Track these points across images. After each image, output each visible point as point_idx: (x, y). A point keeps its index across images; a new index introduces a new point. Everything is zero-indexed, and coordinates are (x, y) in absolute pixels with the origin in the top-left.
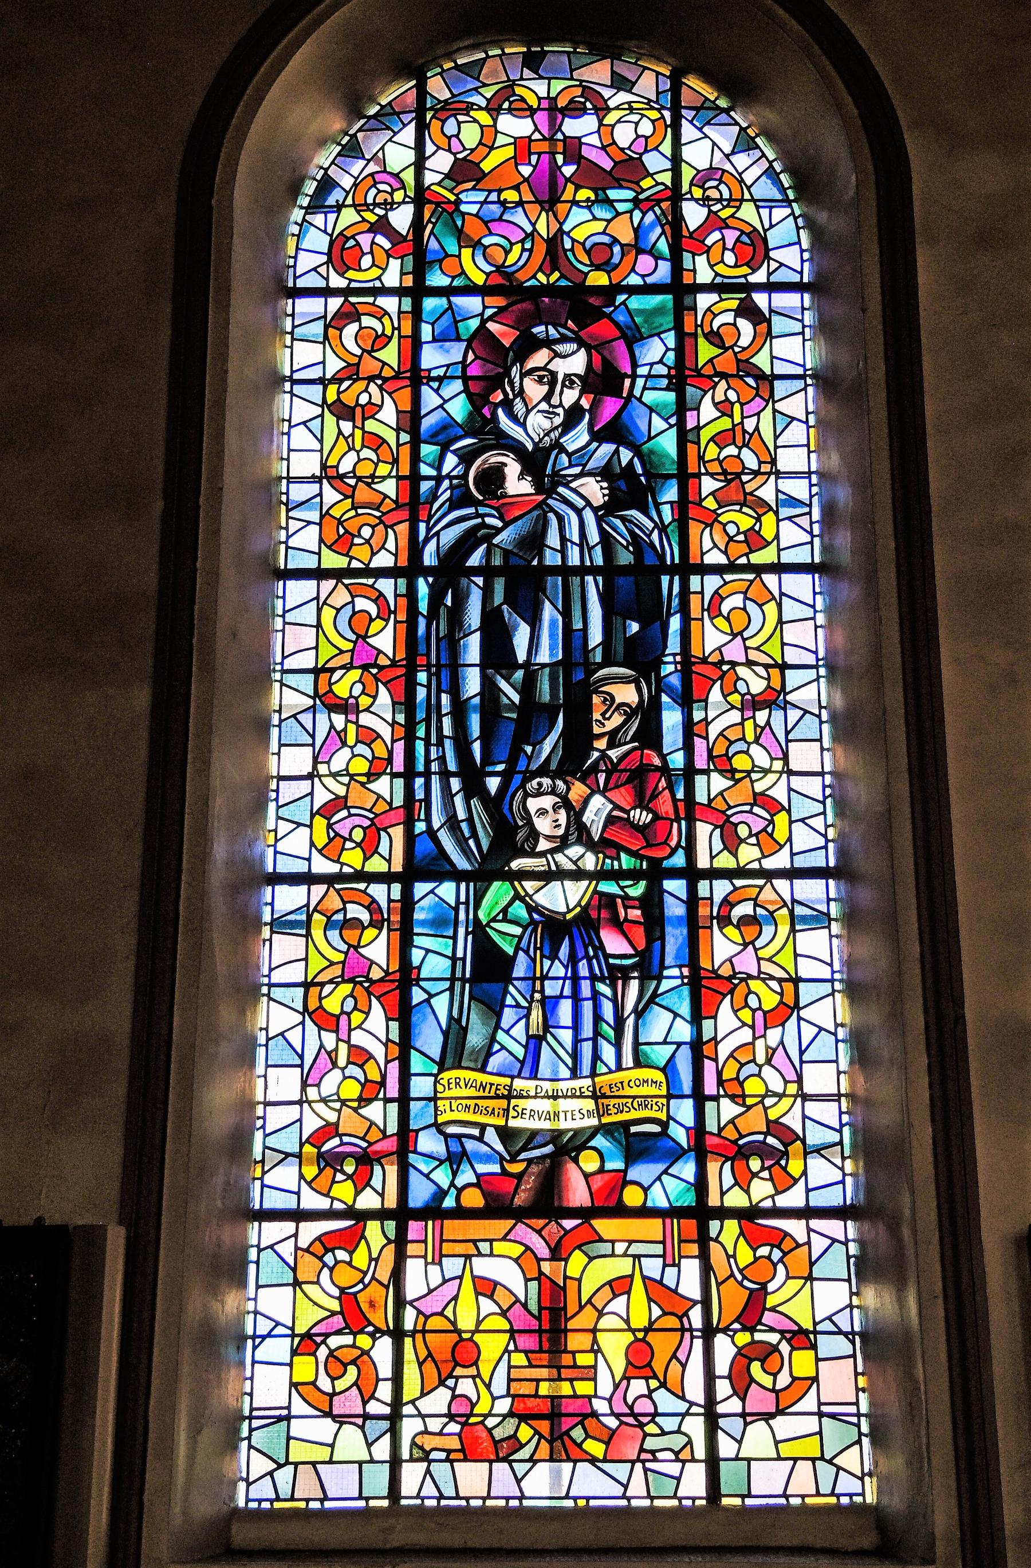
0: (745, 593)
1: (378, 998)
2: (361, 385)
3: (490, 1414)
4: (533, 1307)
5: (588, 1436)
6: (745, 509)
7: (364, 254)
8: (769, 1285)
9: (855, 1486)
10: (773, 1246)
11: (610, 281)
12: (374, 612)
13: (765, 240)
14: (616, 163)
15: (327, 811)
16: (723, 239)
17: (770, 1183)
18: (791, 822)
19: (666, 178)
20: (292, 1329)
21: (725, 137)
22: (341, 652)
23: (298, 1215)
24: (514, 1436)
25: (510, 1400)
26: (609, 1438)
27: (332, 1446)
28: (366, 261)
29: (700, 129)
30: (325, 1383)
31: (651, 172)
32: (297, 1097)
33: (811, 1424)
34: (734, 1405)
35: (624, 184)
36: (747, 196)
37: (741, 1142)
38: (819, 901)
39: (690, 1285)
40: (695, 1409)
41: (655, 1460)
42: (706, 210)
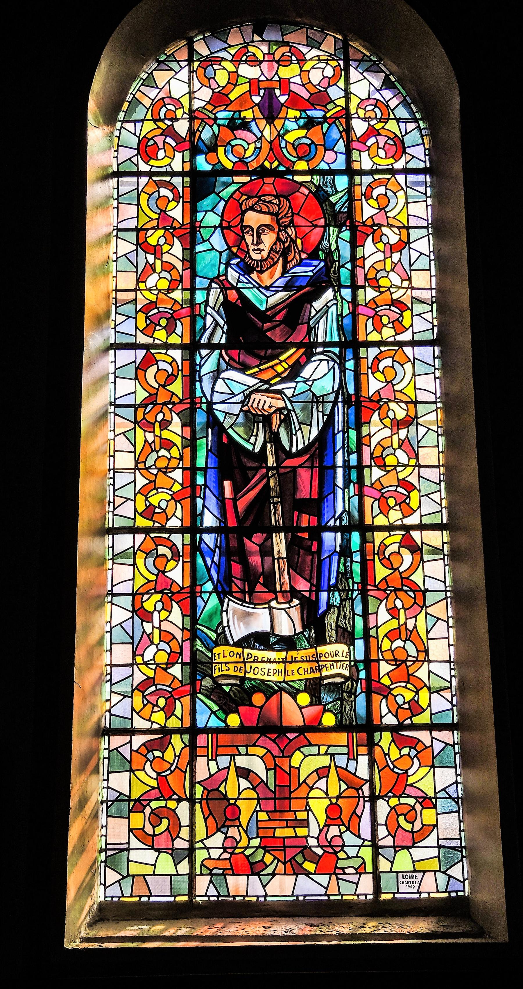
0: (393, 357)
1: (178, 238)
2: (158, 408)
3: (248, 847)
5: (305, 860)
6: (409, 686)
7: (159, 149)
8: (409, 771)
11: (309, 168)
12: (170, 557)
13: (403, 142)
15: (146, 309)
16: (377, 142)
17: (393, 330)
19: (342, 102)
21: (377, 81)
22: (152, 219)
24: (262, 860)
25: (259, 839)
26: (316, 859)
27: (155, 865)
28: (161, 154)
29: (362, 74)
30: (149, 829)
31: (333, 99)
32: (130, 662)
33: (435, 852)
34: (389, 841)
36: (392, 116)
39: (363, 771)
40: (366, 843)
41: (344, 873)
42: (367, 123)
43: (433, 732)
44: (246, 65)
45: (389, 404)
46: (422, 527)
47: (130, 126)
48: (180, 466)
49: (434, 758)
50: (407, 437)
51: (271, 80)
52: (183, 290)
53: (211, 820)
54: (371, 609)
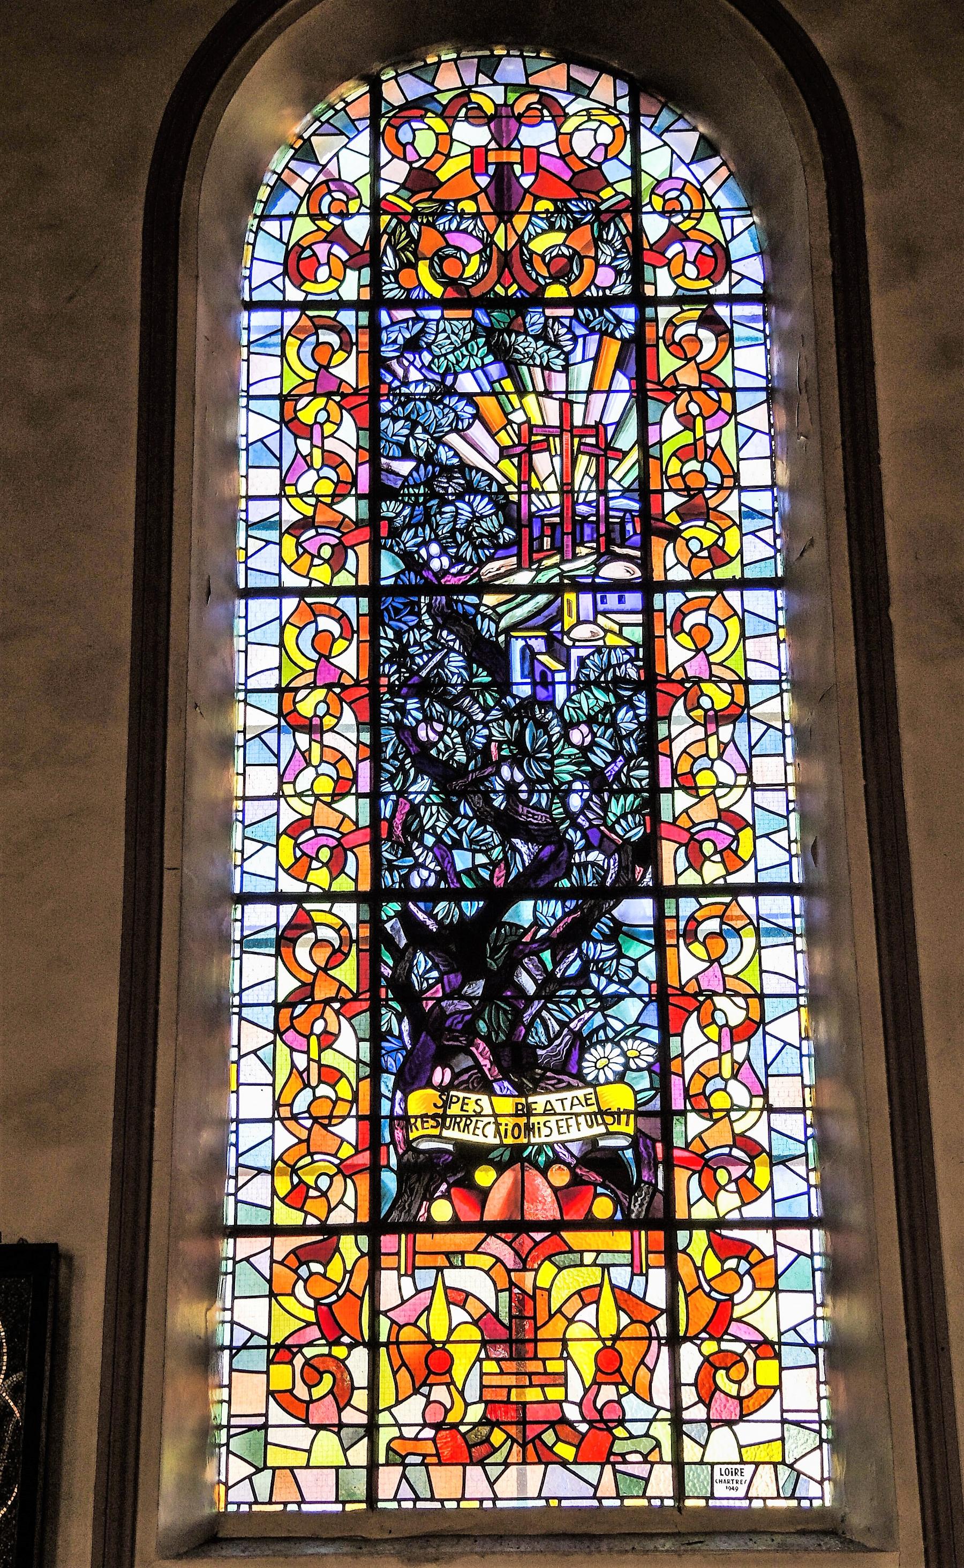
1: (349, 704)
2: (317, 1008)
3: (461, 1423)
4: (504, 1317)
5: (558, 1439)
6: (709, 525)
7: (320, 265)
9: (815, 1491)
10: (740, 1258)
13: (727, 251)
14: (575, 174)
15: (294, 831)
16: (684, 251)
19: (626, 188)
20: (268, 1338)
21: (687, 142)
22: (305, 671)
23: (272, 1231)
24: (487, 1440)
25: (483, 1405)
27: (309, 1451)
28: (323, 273)
30: (301, 1391)
32: (269, 1115)
33: (774, 1431)
34: (699, 1412)
36: (708, 206)
37: (708, 1156)
38: (783, 916)
39: (657, 1295)
41: (625, 1462)
45: (715, 998)
47: (272, 226)
48: (353, 1113)
52: (359, 497)
54: (652, 417)
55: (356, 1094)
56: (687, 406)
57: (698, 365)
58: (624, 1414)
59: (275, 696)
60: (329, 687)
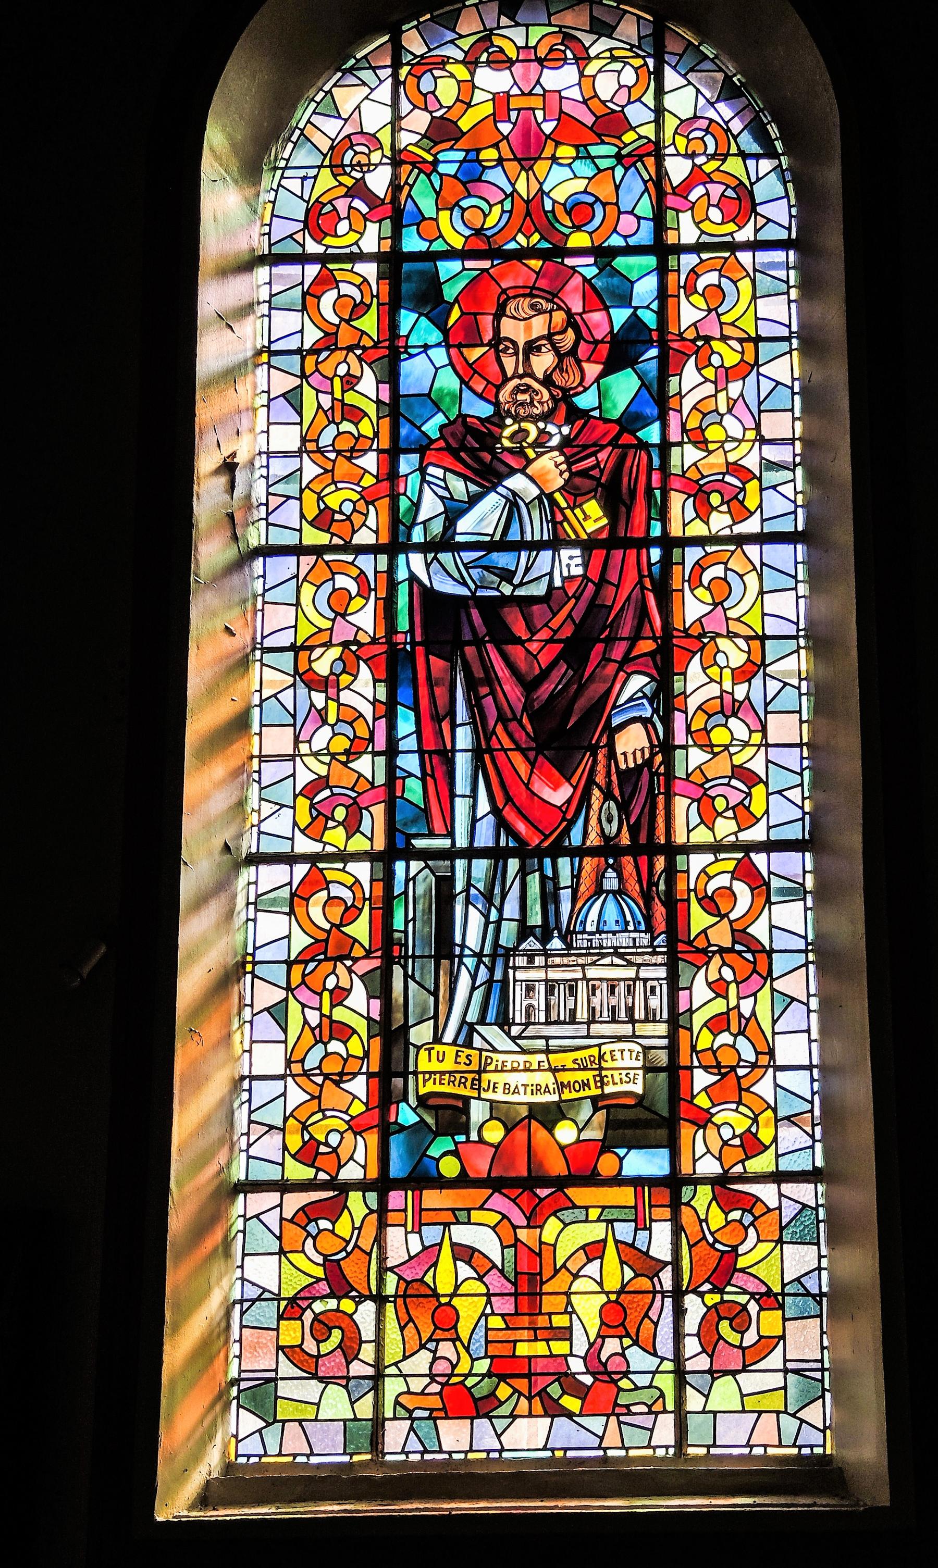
0: (720, 271)
1: (365, 661)
2: (340, 355)
5: (564, 1393)
6: (742, 1109)
7: (340, 219)
9: (817, 1438)
10: (744, 1211)
11: (593, 243)
15: (309, 791)
16: (707, 194)
17: (728, 516)
18: (768, 794)
19: (649, 131)
23: (284, 1187)
24: (493, 1394)
25: (488, 1360)
26: (581, 1392)
27: (318, 1404)
28: (343, 227)
29: (684, 76)
30: (310, 1346)
31: (634, 125)
33: (777, 1380)
34: (703, 1362)
35: (606, 139)
36: (734, 150)
39: (661, 1248)
41: (630, 1413)
43: (783, 1186)
44: (487, 69)
45: (718, 640)
46: (770, 846)
48: (364, 1070)
49: (782, 1229)
50: (747, 697)
51: (530, 94)
53: (410, 1329)
55: (376, 434)
56: (720, 972)
57: (731, 922)
58: (628, 1366)
59: (291, 655)
60: (345, 645)
